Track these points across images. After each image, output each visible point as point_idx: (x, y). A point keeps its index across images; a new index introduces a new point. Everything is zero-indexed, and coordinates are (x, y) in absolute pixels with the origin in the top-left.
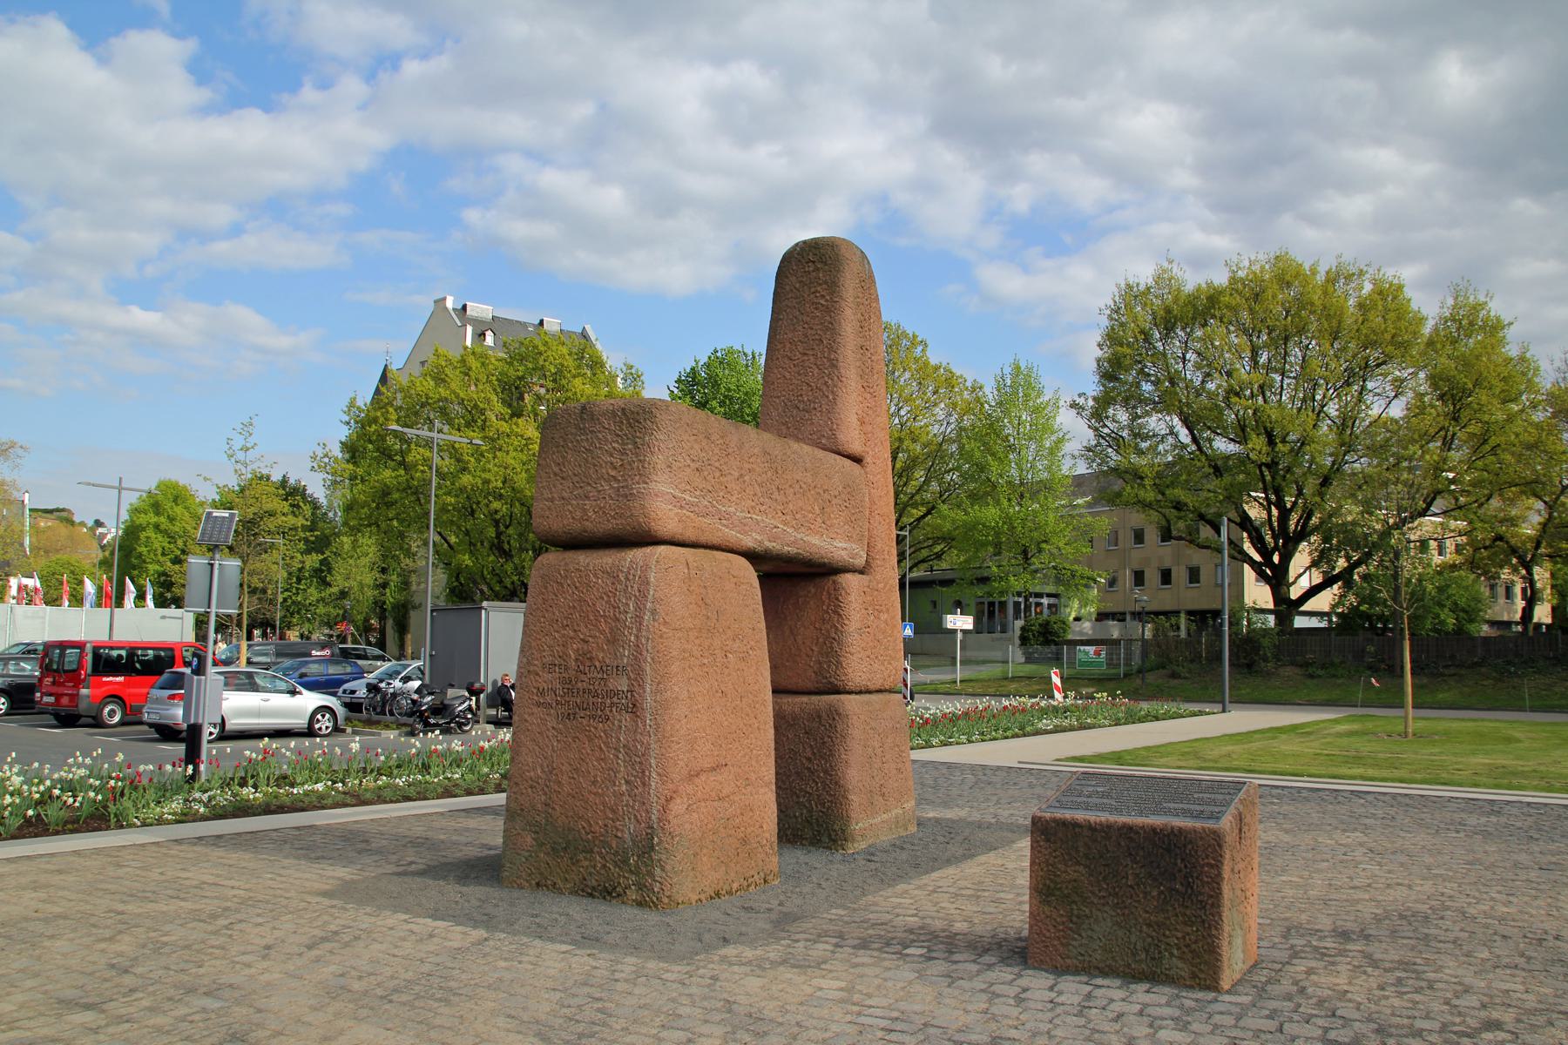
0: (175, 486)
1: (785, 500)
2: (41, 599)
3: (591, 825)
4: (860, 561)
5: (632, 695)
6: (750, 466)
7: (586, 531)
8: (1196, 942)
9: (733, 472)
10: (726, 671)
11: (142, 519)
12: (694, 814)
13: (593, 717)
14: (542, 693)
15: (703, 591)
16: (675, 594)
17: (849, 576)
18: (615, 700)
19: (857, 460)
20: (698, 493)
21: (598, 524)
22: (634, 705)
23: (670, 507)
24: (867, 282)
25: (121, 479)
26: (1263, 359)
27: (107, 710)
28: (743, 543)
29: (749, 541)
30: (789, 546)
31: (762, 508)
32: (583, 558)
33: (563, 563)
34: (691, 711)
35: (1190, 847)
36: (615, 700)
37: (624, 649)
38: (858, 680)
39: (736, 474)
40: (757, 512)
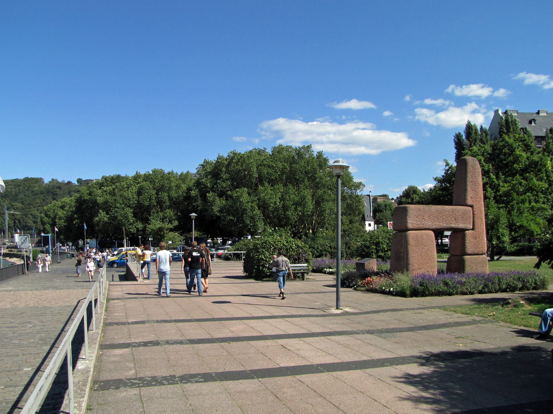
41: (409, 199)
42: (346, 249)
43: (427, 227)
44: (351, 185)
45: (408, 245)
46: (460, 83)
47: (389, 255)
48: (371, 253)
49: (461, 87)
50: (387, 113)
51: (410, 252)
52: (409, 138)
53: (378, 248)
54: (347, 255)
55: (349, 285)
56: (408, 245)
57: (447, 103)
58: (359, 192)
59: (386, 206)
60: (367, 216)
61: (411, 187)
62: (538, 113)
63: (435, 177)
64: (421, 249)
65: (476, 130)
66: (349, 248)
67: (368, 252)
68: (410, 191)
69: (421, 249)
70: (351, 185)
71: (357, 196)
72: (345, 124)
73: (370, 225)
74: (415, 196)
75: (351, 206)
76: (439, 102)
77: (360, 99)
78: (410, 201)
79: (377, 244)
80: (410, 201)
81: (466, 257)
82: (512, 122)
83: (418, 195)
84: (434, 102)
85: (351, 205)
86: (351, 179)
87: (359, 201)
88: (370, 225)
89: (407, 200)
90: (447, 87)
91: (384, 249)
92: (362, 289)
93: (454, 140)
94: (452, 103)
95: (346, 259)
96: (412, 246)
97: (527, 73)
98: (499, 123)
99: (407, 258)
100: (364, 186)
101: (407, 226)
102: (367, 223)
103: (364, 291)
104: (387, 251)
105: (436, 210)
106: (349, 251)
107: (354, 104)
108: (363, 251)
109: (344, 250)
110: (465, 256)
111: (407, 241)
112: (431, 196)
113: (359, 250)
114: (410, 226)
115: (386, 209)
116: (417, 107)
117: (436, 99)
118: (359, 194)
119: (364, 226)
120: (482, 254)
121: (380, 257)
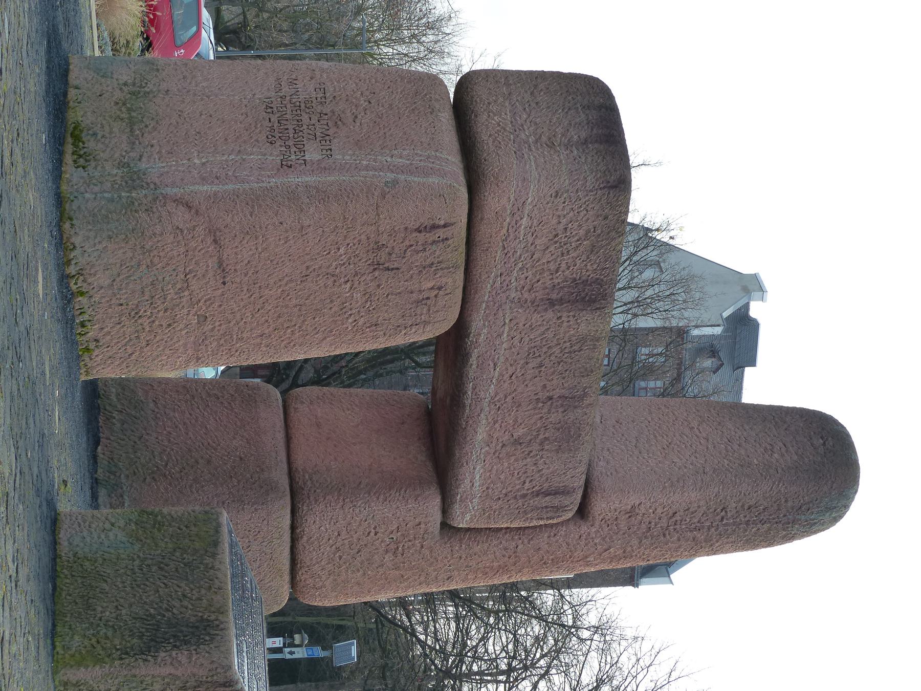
3: (150, 133)
4: (463, 519)
5: (301, 164)
7: (476, 116)
8: (104, 649)
10: (330, 282)
12: (172, 236)
13: (272, 129)
16: (417, 206)
17: (438, 500)
18: (293, 149)
19: (583, 511)
20: (530, 239)
22: (291, 167)
23: (512, 199)
28: (475, 316)
29: (478, 324)
30: (474, 389)
33: (437, 97)
34: (287, 231)
35: (207, 638)
36: (293, 149)
37: (351, 155)
38: (310, 519)
40: (512, 333)
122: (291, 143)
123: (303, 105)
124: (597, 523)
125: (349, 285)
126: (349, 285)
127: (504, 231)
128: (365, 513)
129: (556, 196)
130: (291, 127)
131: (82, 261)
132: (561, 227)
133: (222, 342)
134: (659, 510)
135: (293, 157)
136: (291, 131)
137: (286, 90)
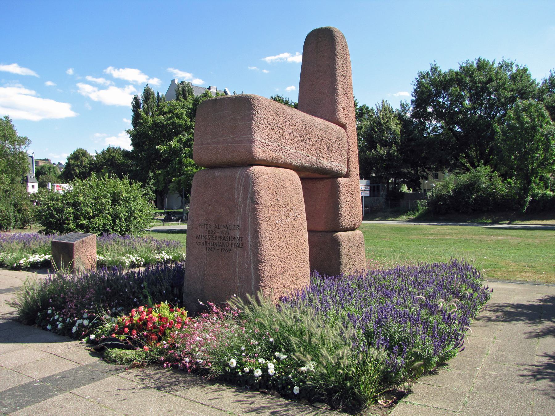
0: (82, 150)
1: (312, 144)
2: (169, 190)
6: (296, 128)
9: (288, 130)
11: (72, 162)
14: (198, 237)
15: (276, 187)
18: (233, 242)
21: (222, 157)
24: (344, 47)
25: (96, 151)
26: (51, 394)
27: (419, 173)
29: (298, 161)
31: (302, 148)
32: (218, 173)
36: (233, 242)
39: (290, 131)
41: (78, 161)
42: (14, 213)
43: (287, 159)
44: (13, 139)
45: (257, 207)
46: (118, 66)
47: (96, 223)
48: (65, 220)
49: (118, 70)
50: (49, 83)
51: (263, 225)
52: (72, 109)
53: (77, 212)
54: (17, 221)
55: (67, 328)
56: (257, 207)
57: (108, 82)
58: (23, 149)
59: (49, 169)
60: (31, 177)
61: (79, 149)
62: (209, 88)
63: (127, 129)
64: (283, 217)
65: (153, 94)
66: (19, 211)
67: (59, 220)
68: (79, 153)
69: (283, 217)
70: (13, 139)
71: (21, 152)
72: (5, 87)
73: (33, 187)
74: (84, 158)
75: (13, 163)
76: (101, 81)
77: (21, 64)
78: (79, 164)
79: (75, 205)
80: (79, 164)
81: (342, 235)
82: (188, 91)
83: (87, 158)
84: (95, 80)
85: (13, 162)
86: (14, 132)
87: (24, 158)
88: (33, 187)
89: (76, 163)
90: (106, 68)
91: (88, 213)
92: (130, 354)
93: (132, 103)
94: (113, 83)
95: (14, 228)
96: (265, 209)
97: (175, 69)
98: (176, 91)
99: (257, 245)
100: (30, 142)
101: (251, 152)
102: (30, 185)
103: (142, 365)
104: (93, 217)
105: (302, 121)
106: (19, 216)
107: (14, 69)
108: (50, 217)
109: (11, 214)
110: (338, 234)
111: (253, 193)
112: (105, 159)
113: (43, 216)
114: (259, 152)
115: (49, 172)
116: (79, 81)
117: (97, 78)
118: (24, 151)
119: (26, 187)
120: (353, 229)
121: (81, 227)
122: (230, 243)
123: (210, 234)
124: (346, 122)
125: (288, 218)
126: (288, 218)
127: (269, 151)
128: (343, 205)
129: (259, 127)
130: (222, 241)
131: (134, 184)
132: (269, 126)
133: (304, 268)
134: (343, 99)
135: (238, 242)
136: (224, 241)
137: (202, 240)
